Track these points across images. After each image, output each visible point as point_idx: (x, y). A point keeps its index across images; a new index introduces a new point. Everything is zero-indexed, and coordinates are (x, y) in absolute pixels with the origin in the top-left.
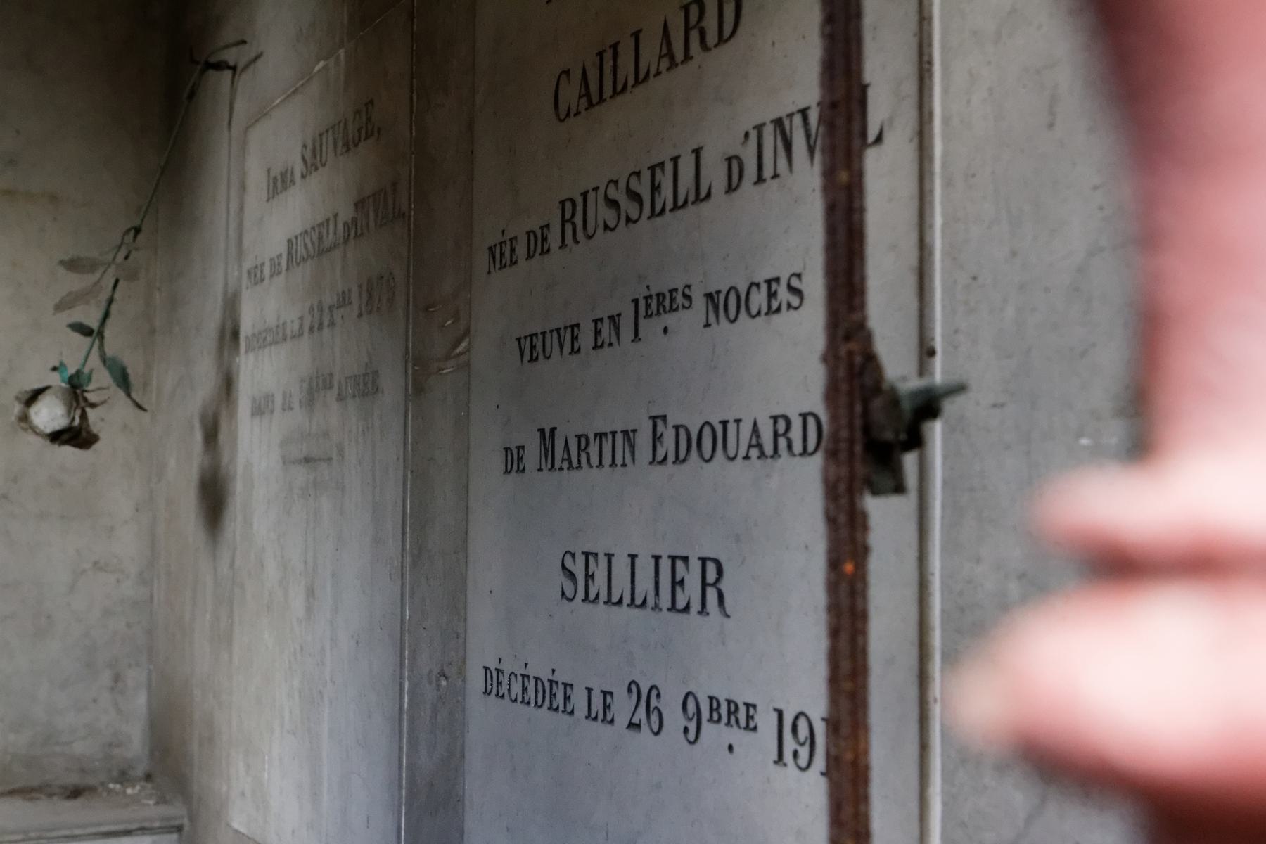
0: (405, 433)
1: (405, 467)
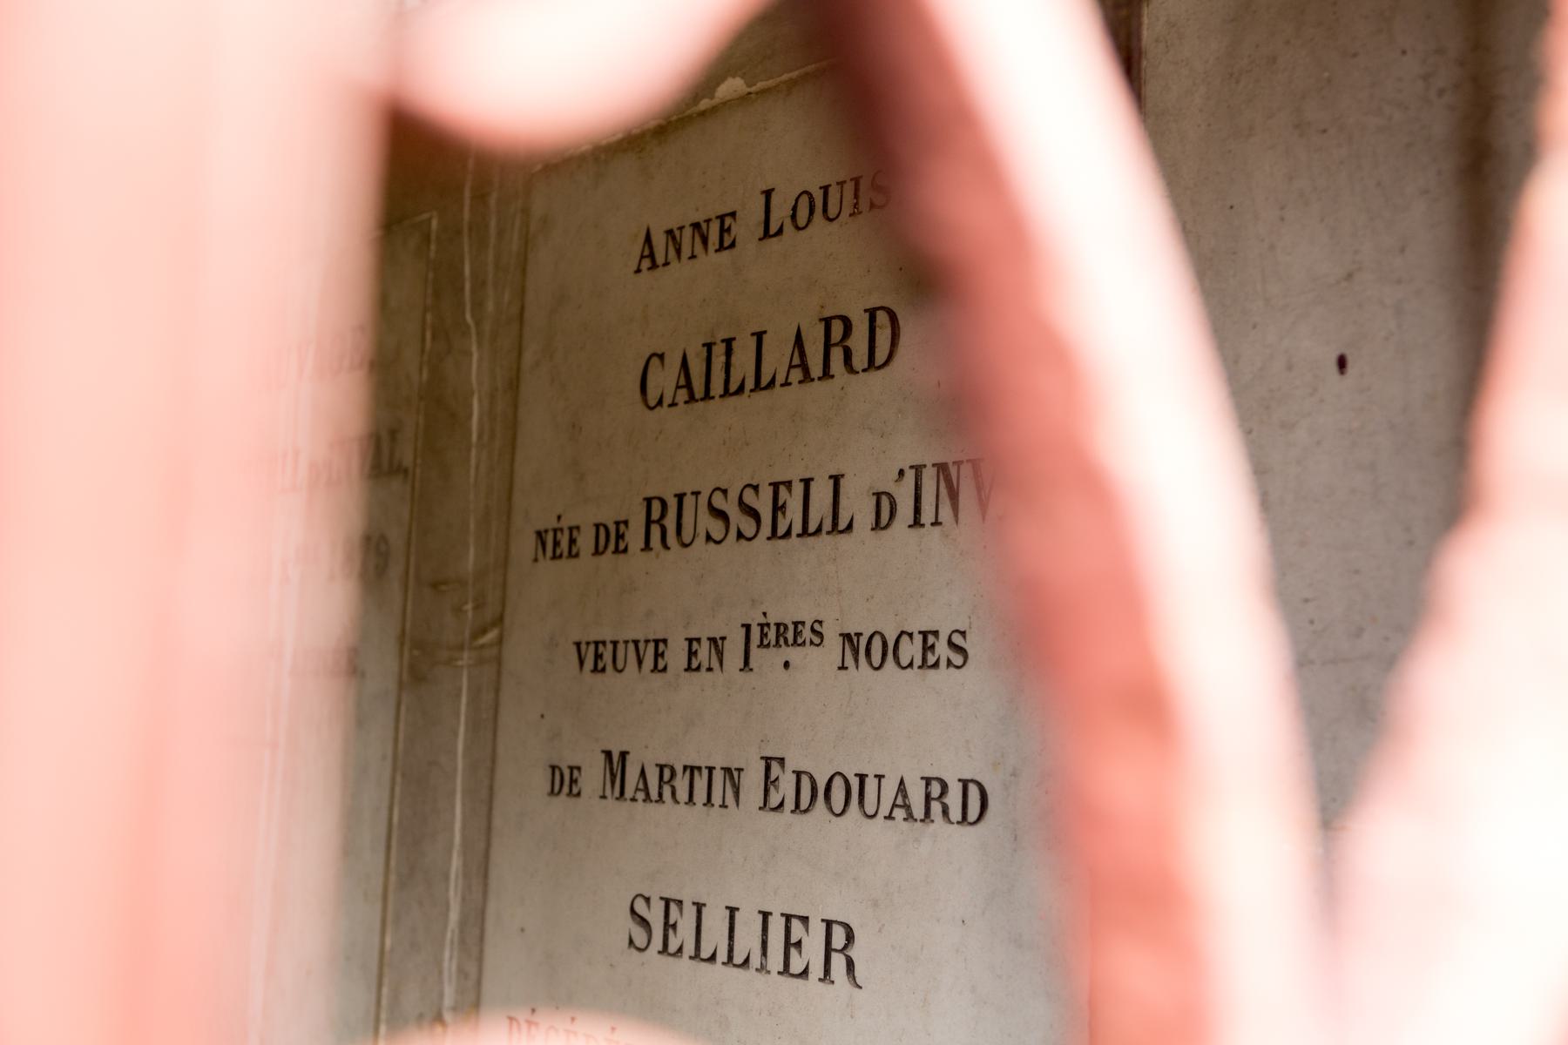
0: (397, 729)
1: (394, 770)
